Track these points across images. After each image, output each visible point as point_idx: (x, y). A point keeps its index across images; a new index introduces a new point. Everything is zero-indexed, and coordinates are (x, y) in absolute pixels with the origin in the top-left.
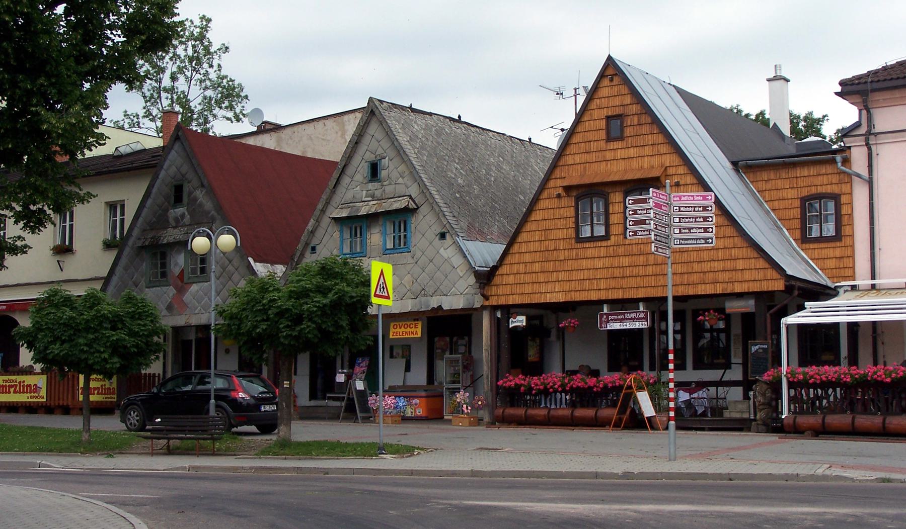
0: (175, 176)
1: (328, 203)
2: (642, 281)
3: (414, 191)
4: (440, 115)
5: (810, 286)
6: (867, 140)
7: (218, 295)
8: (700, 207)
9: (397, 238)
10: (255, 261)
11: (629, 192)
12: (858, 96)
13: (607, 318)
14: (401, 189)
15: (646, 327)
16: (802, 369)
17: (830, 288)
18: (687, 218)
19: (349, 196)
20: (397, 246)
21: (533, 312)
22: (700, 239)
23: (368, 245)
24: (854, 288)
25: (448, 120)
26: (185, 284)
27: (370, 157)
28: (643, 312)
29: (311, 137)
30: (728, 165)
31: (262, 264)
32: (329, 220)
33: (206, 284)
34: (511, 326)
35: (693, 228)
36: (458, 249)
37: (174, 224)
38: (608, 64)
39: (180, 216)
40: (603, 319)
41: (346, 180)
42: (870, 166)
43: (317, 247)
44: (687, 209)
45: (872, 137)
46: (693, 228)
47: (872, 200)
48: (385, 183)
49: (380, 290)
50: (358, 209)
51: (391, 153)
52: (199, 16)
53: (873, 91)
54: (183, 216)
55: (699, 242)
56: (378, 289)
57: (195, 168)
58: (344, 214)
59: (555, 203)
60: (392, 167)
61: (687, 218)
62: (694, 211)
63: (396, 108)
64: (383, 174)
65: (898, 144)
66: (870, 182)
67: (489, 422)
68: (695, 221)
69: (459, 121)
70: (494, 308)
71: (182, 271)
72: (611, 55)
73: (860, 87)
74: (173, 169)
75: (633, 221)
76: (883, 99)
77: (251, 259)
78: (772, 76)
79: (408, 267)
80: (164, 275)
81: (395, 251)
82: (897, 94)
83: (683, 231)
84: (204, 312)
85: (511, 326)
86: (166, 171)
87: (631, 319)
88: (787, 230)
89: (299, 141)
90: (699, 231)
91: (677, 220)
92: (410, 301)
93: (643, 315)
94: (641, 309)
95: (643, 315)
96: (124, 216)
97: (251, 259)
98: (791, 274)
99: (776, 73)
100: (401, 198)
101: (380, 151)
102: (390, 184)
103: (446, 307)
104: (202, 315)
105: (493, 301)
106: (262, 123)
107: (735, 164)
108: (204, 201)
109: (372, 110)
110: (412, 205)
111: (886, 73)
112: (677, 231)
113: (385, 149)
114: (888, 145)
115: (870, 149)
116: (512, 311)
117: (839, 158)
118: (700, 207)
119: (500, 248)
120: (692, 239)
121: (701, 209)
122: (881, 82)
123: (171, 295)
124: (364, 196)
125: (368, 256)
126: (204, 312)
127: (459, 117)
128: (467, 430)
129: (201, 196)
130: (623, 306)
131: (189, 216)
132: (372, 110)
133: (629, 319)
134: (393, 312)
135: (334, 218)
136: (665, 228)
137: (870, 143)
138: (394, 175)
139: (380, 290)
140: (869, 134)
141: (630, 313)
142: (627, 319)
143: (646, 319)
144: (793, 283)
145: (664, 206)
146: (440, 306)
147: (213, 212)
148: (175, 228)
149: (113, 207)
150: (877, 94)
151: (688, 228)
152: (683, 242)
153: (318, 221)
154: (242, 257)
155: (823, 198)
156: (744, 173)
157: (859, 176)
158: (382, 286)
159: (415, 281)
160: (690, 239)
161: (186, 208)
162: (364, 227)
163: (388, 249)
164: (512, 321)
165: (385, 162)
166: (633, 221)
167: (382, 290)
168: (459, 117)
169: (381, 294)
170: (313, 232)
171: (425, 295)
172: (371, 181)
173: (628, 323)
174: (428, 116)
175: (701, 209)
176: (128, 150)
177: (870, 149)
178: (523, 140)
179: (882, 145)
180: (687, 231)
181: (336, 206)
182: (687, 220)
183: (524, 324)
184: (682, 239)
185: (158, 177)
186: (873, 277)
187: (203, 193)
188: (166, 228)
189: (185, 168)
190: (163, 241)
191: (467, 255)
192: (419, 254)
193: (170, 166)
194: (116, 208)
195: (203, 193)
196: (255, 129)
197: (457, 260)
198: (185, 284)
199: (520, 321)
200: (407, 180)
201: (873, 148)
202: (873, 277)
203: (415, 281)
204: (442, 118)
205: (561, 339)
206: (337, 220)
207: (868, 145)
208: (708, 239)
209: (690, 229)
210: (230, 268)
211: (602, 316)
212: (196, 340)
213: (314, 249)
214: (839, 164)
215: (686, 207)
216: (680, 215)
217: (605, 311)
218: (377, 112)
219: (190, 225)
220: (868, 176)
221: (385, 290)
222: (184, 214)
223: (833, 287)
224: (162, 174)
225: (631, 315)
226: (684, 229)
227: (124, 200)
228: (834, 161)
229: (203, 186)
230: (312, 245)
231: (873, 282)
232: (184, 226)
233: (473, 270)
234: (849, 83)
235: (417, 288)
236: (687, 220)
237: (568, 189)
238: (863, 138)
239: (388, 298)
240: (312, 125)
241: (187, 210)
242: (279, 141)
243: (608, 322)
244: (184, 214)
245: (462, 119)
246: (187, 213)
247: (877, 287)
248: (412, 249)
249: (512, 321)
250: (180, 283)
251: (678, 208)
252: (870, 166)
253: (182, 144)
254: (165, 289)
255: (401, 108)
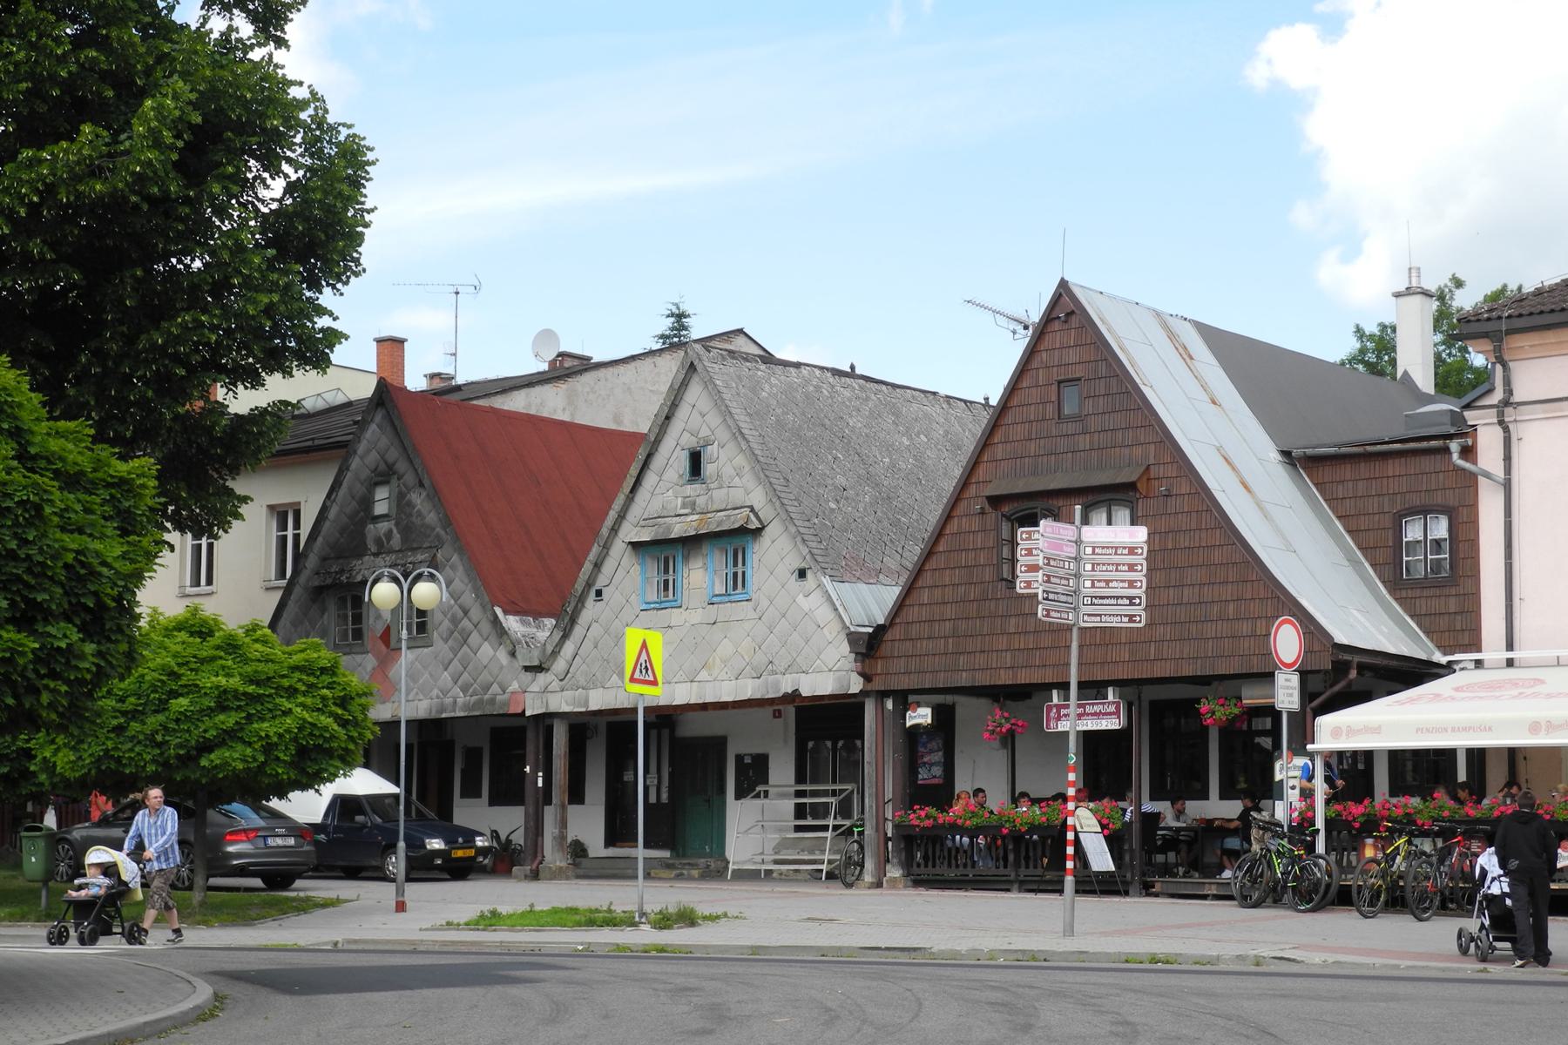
0: (376, 469)
1: (622, 516)
2: (1062, 658)
3: (758, 498)
4: (815, 367)
5: (1394, 663)
6: (1501, 414)
7: (446, 669)
8: (1125, 548)
9: (730, 577)
10: (506, 612)
11: (1091, 505)
12: (1486, 340)
13: (1058, 712)
14: (737, 496)
15: (1117, 727)
16: (1394, 800)
17: (1439, 665)
18: (1104, 564)
19: (655, 507)
20: (730, 590)
21: (939, 699)
22: (1122, 597)
23: (685, 587)
24: (1479, 664)
25: (829, 375)
26: (393, 650)
27: (689, 441)
28: (1114, 703)
29: (629, 389)
30: (1274, 456)
31: (517, 618)
32: (624, 546)
33: (426, 650)
34: (908, 724)
35: (1112, 581)
36: (825, 598)
37: (374, 549)
38: (1060, 295)
39: (385, 535)
40: (1052, 714)
41: (650, 479)
42: (1508, 458)
43: (605, 595)
44: (1104, 551)
45: (1508, 410)
46: (1112, 581)
47: (1510, 516)
48: (712, 486)
49: (641, 672)
50: (669, 528)
51: (723, 435)
52: (266, 387)
53: (1510, 332)
54: (389, 534)
55: (1120, 601)
56: (638, 670)
57: (409, 456)
58: (645, 537)
59: (976, 524)
60: (722, 458)
61: (1104, 564)
62: (1116, 554)
63: (734, 358)
64: (708, 469)
65: (1556, 421)
66: (1507, 486)
67: (872, 883)
68: (1117, 570)
69: (851, 374)
70: (882, 695)
71: (388, 629)
72: (1066, 278)
73: (1489, 327)
74: (373, 457)
75: (1026, 566)
76: (1531, 346)
77: (498, 611)
78: (1402, 288)
79: (747, 625)
80: (358, 634)
81: (726, 599)
82: (1551, 337)
83: (1097, 584)
84: (421, 697)
85: (908, 724)
86: (362, 458)
87: (1095, 714)
88: (1372, 565)
89: (609, 396)
90: (1121, 585)
91: (1089, 567)
92: (750, 681)
93: (1112, 709)
94: (1111, 697)
95: (1112, 709)
96: (299, 529)
97: (498, 611)
98: (1345, 641)
99: (1410, 282)
100: (737, 511)
101: (705, 432)
102: (721, 487)
103: (806, 692)
104: (420, 704)
105: (878, 685)
106: (558, 356)
107: (1286, 454)
108: (423, 510)
109: (692, 363)
110: (754, 524)
111: (1538, 299)
112: (1088, 584)
113: (713, 427)
114: (1537, 423)
115: (1506, 430)
116: (911, 698)
117: (1454, 446)
118: (1125, 548)
119: (891, 594)
120: (1111, 597)
121: (1126, 551)
122: (1556, 313)
123: (369, 668)
124: (679, 506)
125: (684, 607)
126: (421, 697)
127: (852, 367)
128: (828, 895)
129: (419, 502)
130: (1098, 692)
131: (398, 536)
132: (692, 363)
133: (1092, 714)
134: (722, 700)
135: (630, 543)
136: (1068, 579)
137: (1506, 420)
138: (728, 471)
139: (641, 672)
140: (1506, 403)
141: (1093, 704)
142: (1088, 715)
143: (1117, 713)
144: (1347, 657)
145: (1067, 545)
146: (492, 728)
147: (438, 529)
148: (376, 555)
149: (283, 515)
150: (1517, 336)
151: (1105, 581)
152: (1095, 601)
153: (606, 547)
154: (483, 607)
155: (1431, 512)
156: (1304, 468)
157: (1487, 475)
158: (644, 665)
159: (757, 648)
160: (1107, 597)
161: (393, 522)
162: (679, 559)
163: (717, 596)
164: (910, 717)
165: (710, 452)
166: (1026, 566)
167: (644, 671)
168: (852, 367)
169: (642, 678)
170: (598, 566)
171: (774, 673)
172: (690, 481)
173: (1089, 722)
174: (791, 369)
175: (1126, 551)
176: (320, 405)
177: (1506, 430)
178: (971, 402)
179: (1528, 424)
180: (1103, 584)
181: (635, 521)
182: (1104, 568)
183: (929, 721)
184: (1096, 597)
185: (348, 469)
186: (1510, 646)
187: (422, 497)
188: (360, 556)
189: (393, 454)
190: (355, 578)
191: (838, 606)
192: (764, 603)
193: (368, 451)
194: (286, 513)
195: (422, 497)
196: (544, 367)
197: (824, 613)
198: (393, 650)
199: (921, 716)
200: (748, 480)
201: (1511, 427)
202: (1510, 646)
203: (757, 648)
204: (817, 372)
205: (1010, 747)
206: (636, 546)
207: (1501, 422)
208: (1134, 598)
209: (1107, 582)
210: (466, 623)
211: (1050, 709)
212: (419, 743)
213: (599, 593)
214: (1455, 456)
215: (1103, 548)
216: (1094, 559)
217: (1055, 700)
218: (699, 368)
219: (400, 551)
220: (1503, 476)
221: (650, 671)
222: (390, 531)
223: (1444, 663)
224: (355, 463)
225: (1095, 707)
226: (1099, 581)
227: (299, 503)
228: (1447, 450)
229: (421, 485)
230: (597, 586)
231: (1510, 655)
232: (390, 552)
233: (847, 631)
234: (1473, 318)
235: (761, 658)
236: (1104, 568)
237: (995, 501)
238: (1495, 410)
239: (654, 683)
240: (633, 365)
241: (397, 524)
242: (571, 399)
243: (1059, 718)
244: (390, 531)
245: (858, 371)
246: (395, 531)
247: (1516, 663)
248: (754, 597)
249: (910, 717)
250: (383, 648)
251: (1091, 549)
252: (1508, 458)
253: (388, 412)
254: (359, 658)
255: (743, 358)
